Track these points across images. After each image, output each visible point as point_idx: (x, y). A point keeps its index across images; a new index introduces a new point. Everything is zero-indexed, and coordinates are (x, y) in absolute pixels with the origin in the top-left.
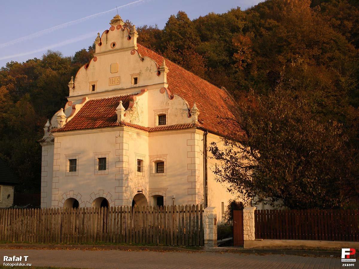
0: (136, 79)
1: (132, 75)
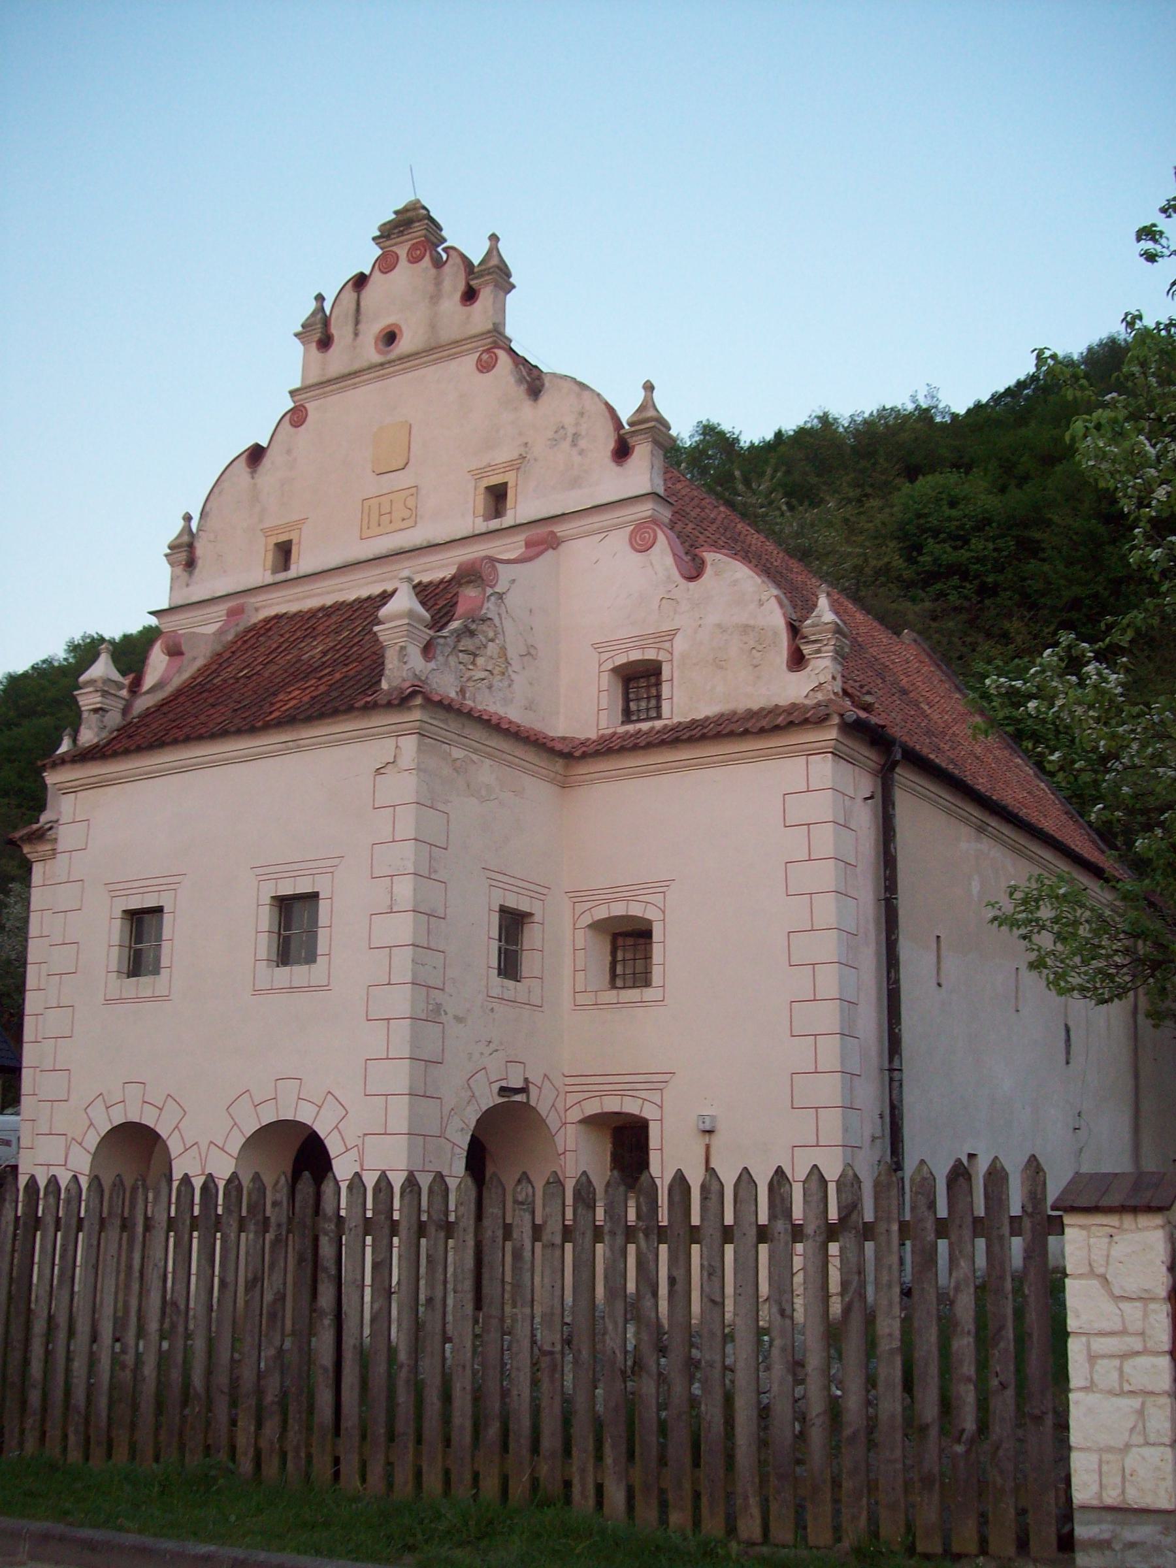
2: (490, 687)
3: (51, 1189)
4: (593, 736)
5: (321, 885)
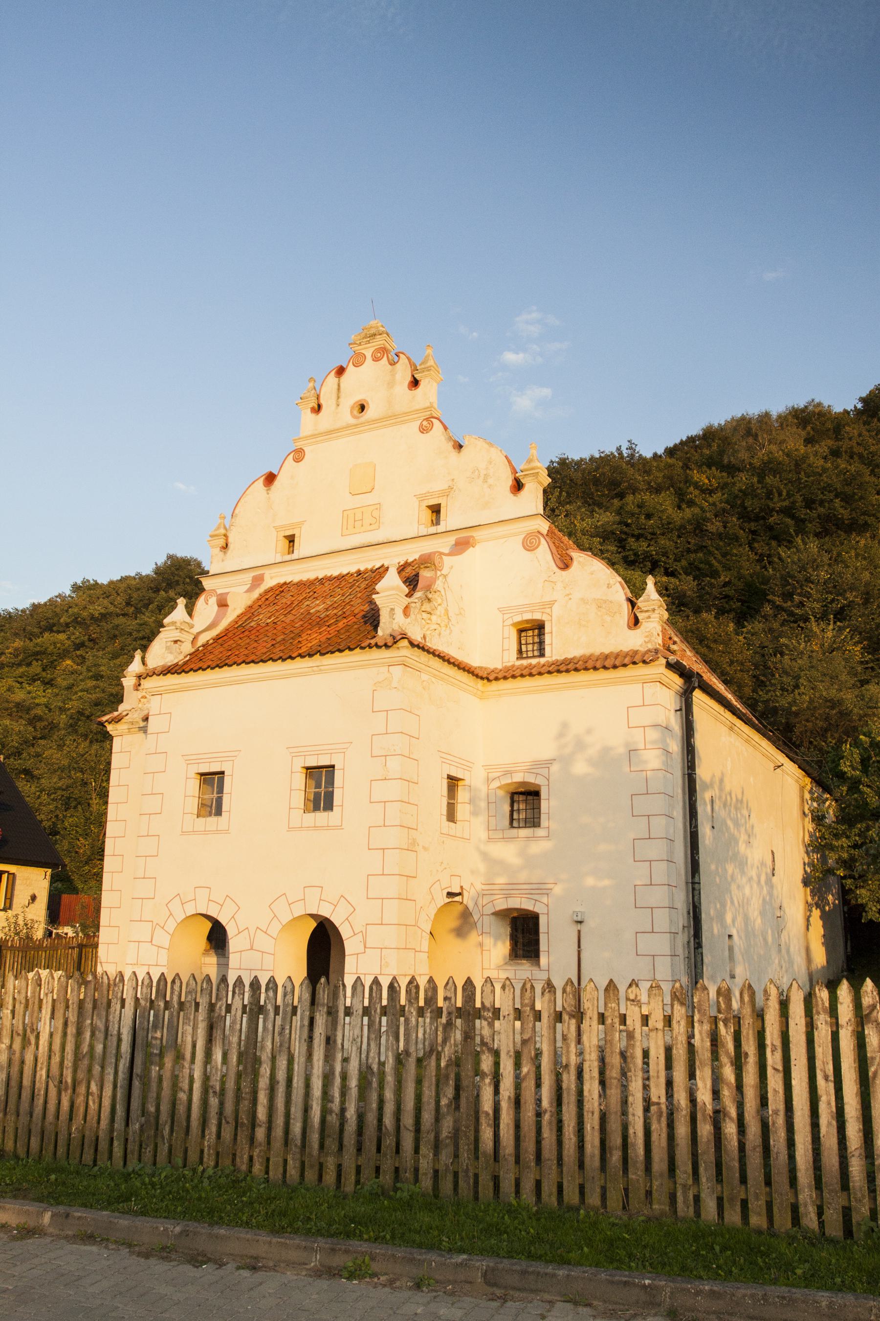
0: (436, 510)
1: (421, 498)
2: (440, 634)
3: (271, 985)
4: (500, 667)
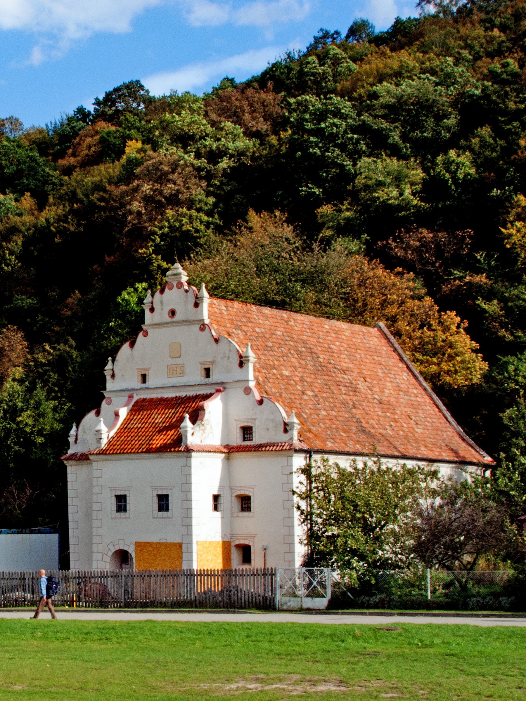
0: (208, 372)
1: (202, 363)
5: (169, 493)
